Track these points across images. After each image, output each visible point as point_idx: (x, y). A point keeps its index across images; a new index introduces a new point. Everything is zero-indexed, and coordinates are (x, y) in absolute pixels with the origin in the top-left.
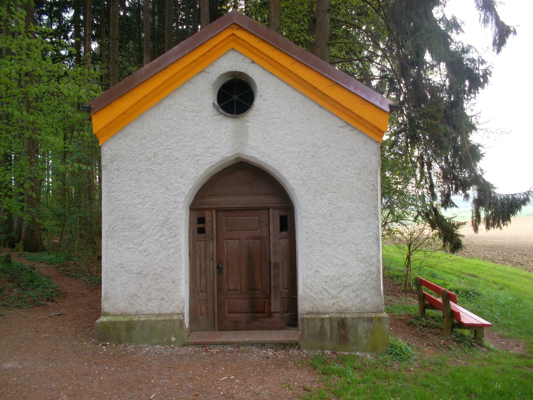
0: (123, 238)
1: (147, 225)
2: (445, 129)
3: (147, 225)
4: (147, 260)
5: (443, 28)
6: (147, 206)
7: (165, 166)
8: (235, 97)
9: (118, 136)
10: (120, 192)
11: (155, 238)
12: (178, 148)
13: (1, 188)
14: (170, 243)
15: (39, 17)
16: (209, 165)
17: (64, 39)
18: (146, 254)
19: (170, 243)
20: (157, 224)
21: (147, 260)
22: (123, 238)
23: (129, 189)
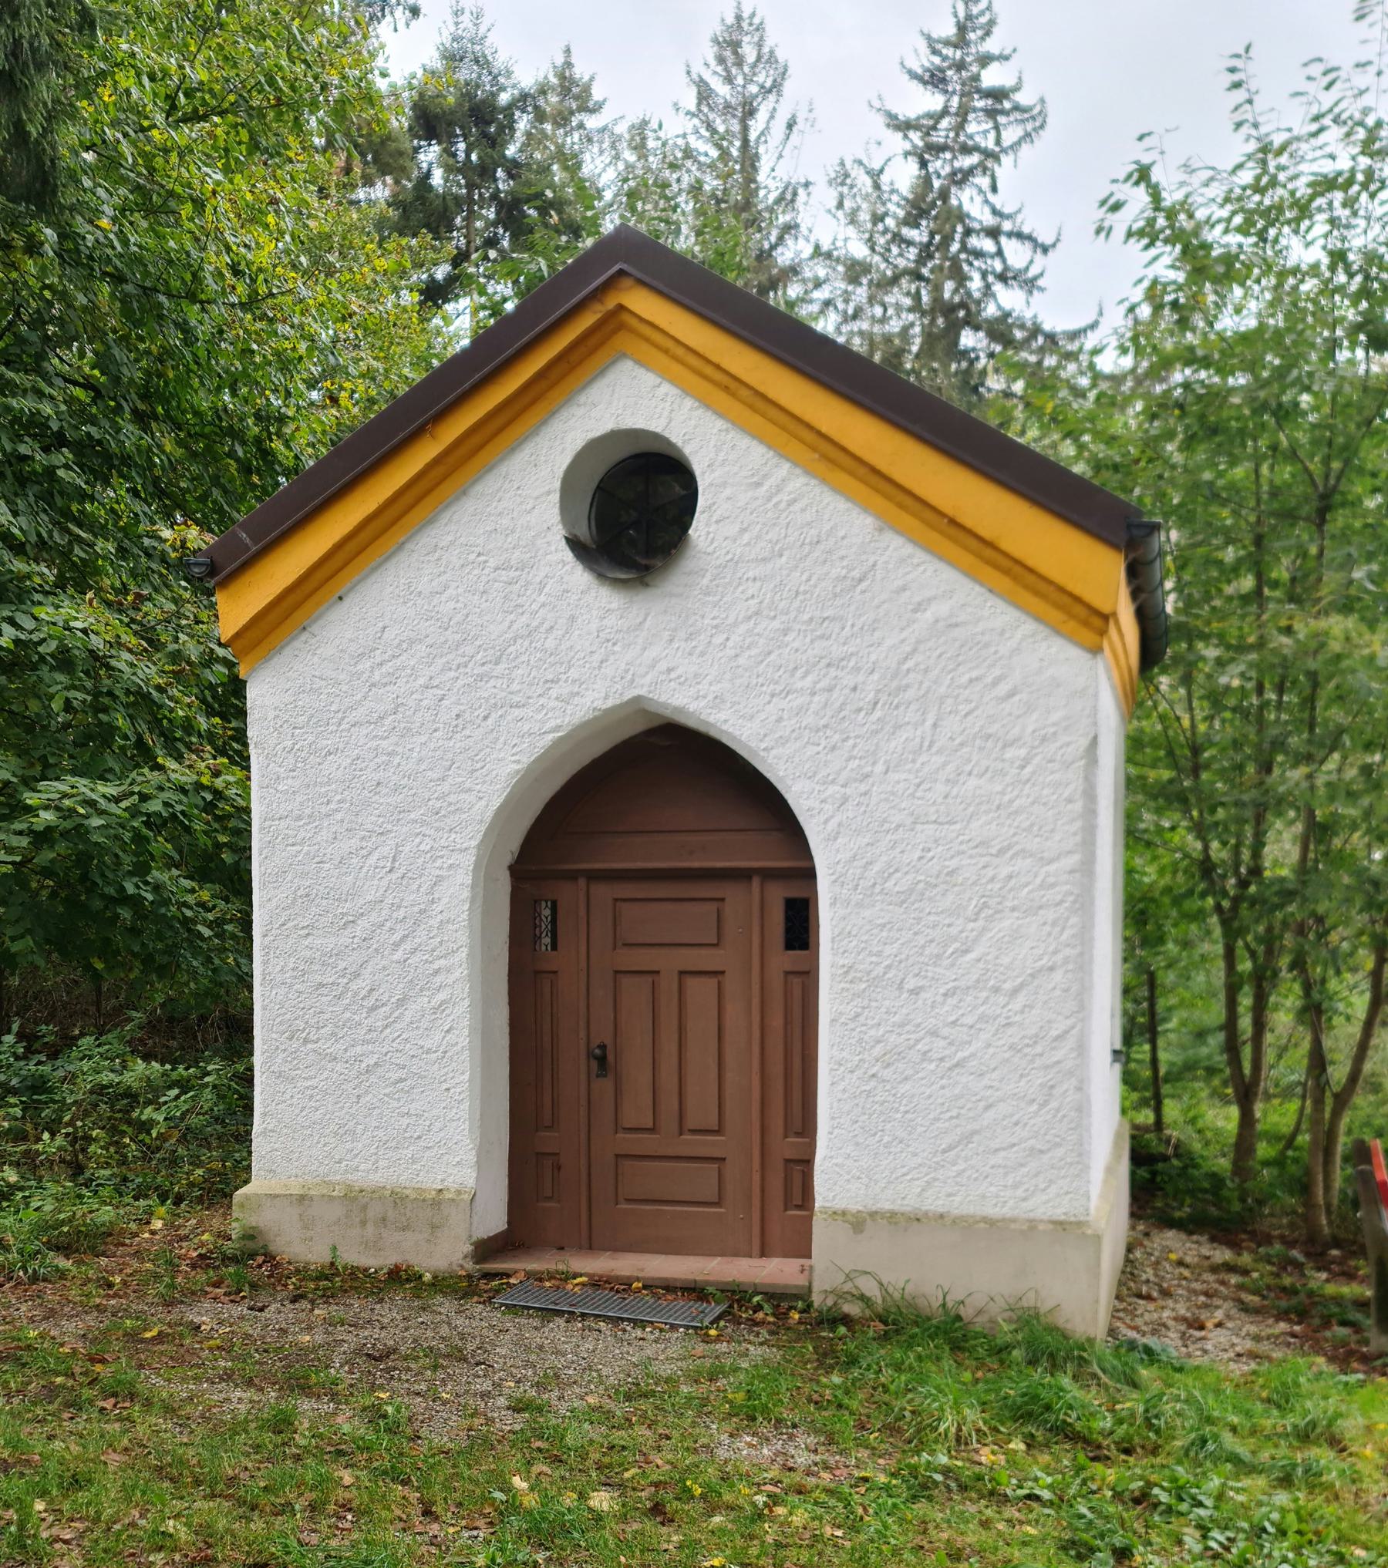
0: (308, 954)
1: (374, 917)
2: (1312, 456)
3: (374, 917)
4: (373, 1064)
5: (1169, 609)
6: (372, 860)
7: (423, 739)
8: (636, 514)
9: (287, 651)
10: (299, 818)
11: (399, 955)
12: (460, 682)
13: (1, 1209)
14: (437, 972)
15: (66, 554)
16: (551, 736)
17: (149, 1133)
18: (369, 1002)
19: (437, 972)
20: (401, 914)
21: (373, 1064)
22: (308, 954)
23: (324, 810)
